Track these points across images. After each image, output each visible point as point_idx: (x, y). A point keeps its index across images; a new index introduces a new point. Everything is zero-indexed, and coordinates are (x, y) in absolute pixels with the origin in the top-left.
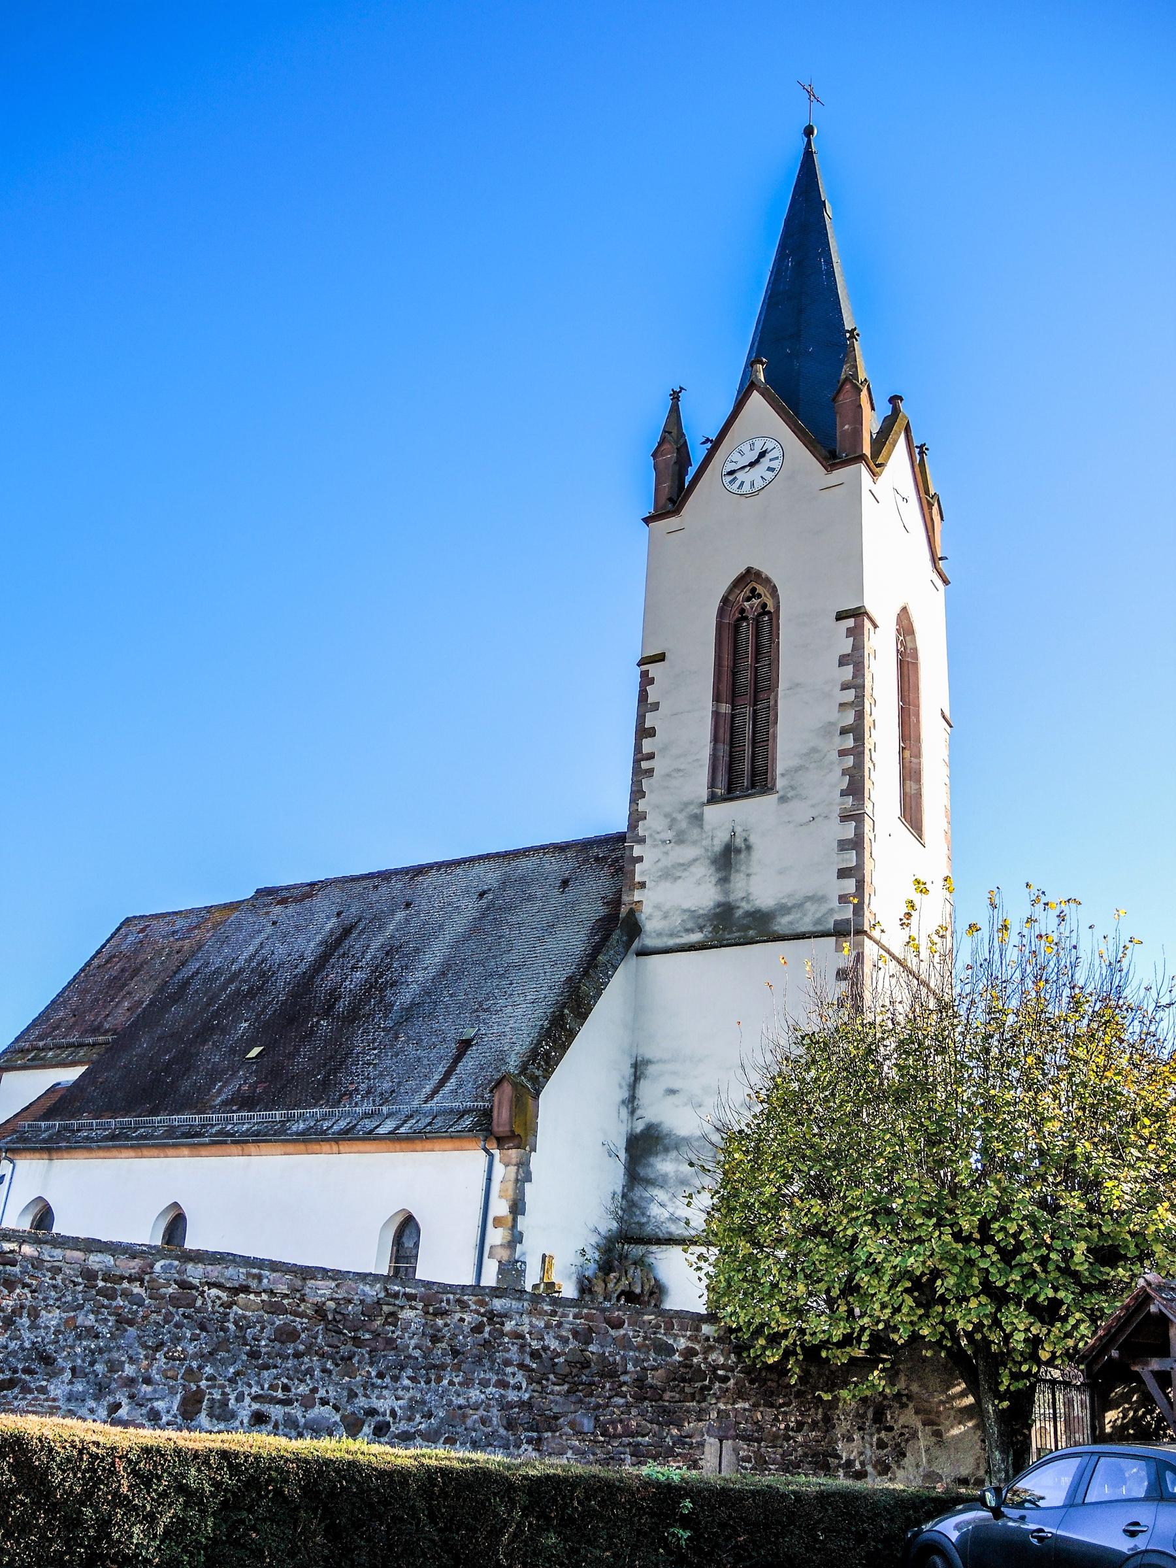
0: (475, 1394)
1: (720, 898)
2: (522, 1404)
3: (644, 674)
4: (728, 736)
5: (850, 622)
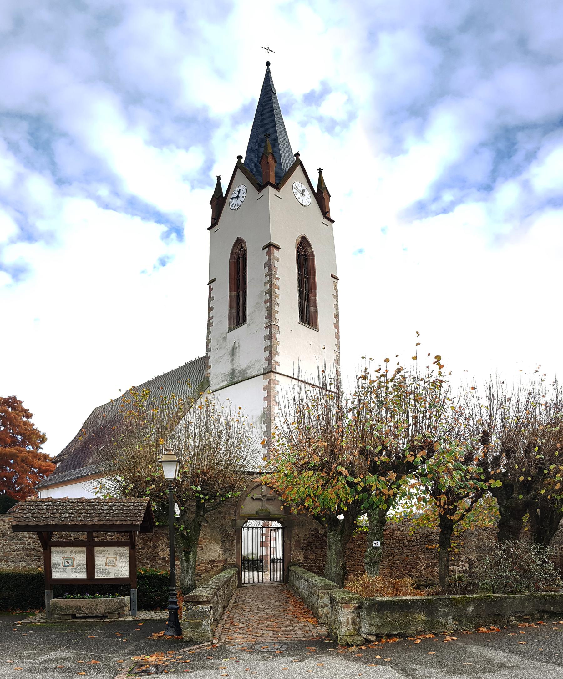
0: (13, 547)
1: (232, 367)
2: (31, 549)
3: (210, 287)
4: (235, 304)
5: (267, 249)
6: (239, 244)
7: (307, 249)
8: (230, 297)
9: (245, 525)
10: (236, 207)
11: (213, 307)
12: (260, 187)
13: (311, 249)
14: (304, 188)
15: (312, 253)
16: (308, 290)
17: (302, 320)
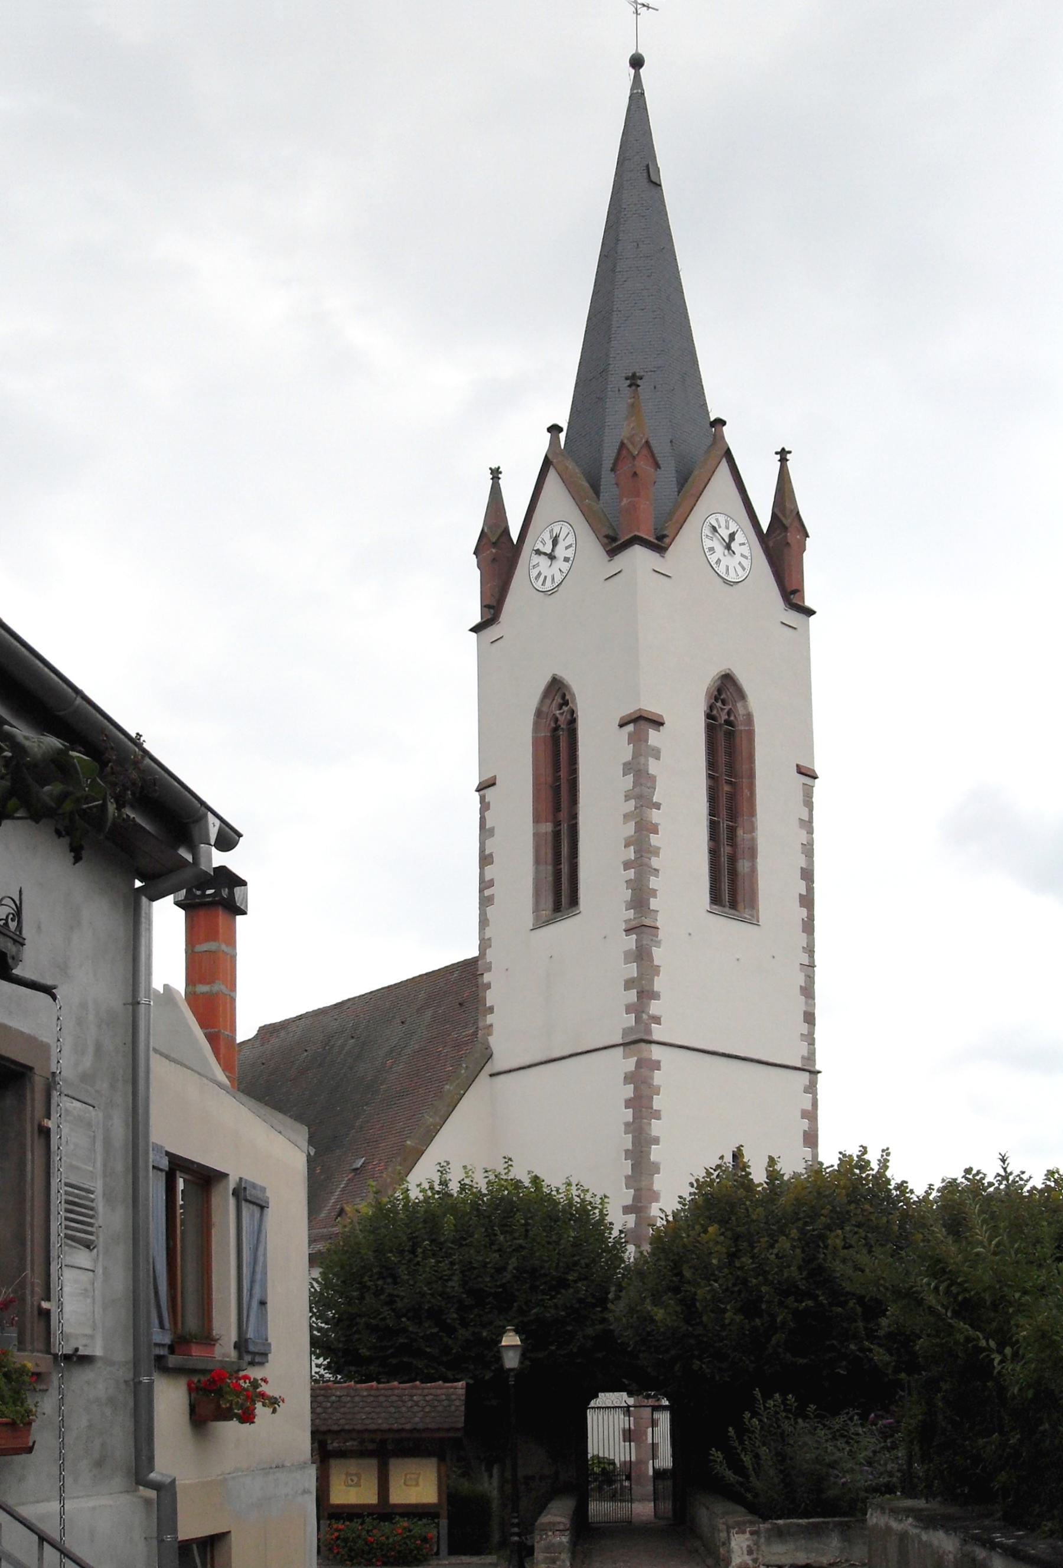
4: (550, 856)
5: (630, 728)
6: (557, 692)
7: (735, 706)
8: (536, 835)
9: (592, 1404)
10: (549, 585)
11: (491, 855)
12: (615, 545)
13: (746, 707)
14: (733, 527)
15: (749, 717)
16: (733, 815)
17: (716, 898)
